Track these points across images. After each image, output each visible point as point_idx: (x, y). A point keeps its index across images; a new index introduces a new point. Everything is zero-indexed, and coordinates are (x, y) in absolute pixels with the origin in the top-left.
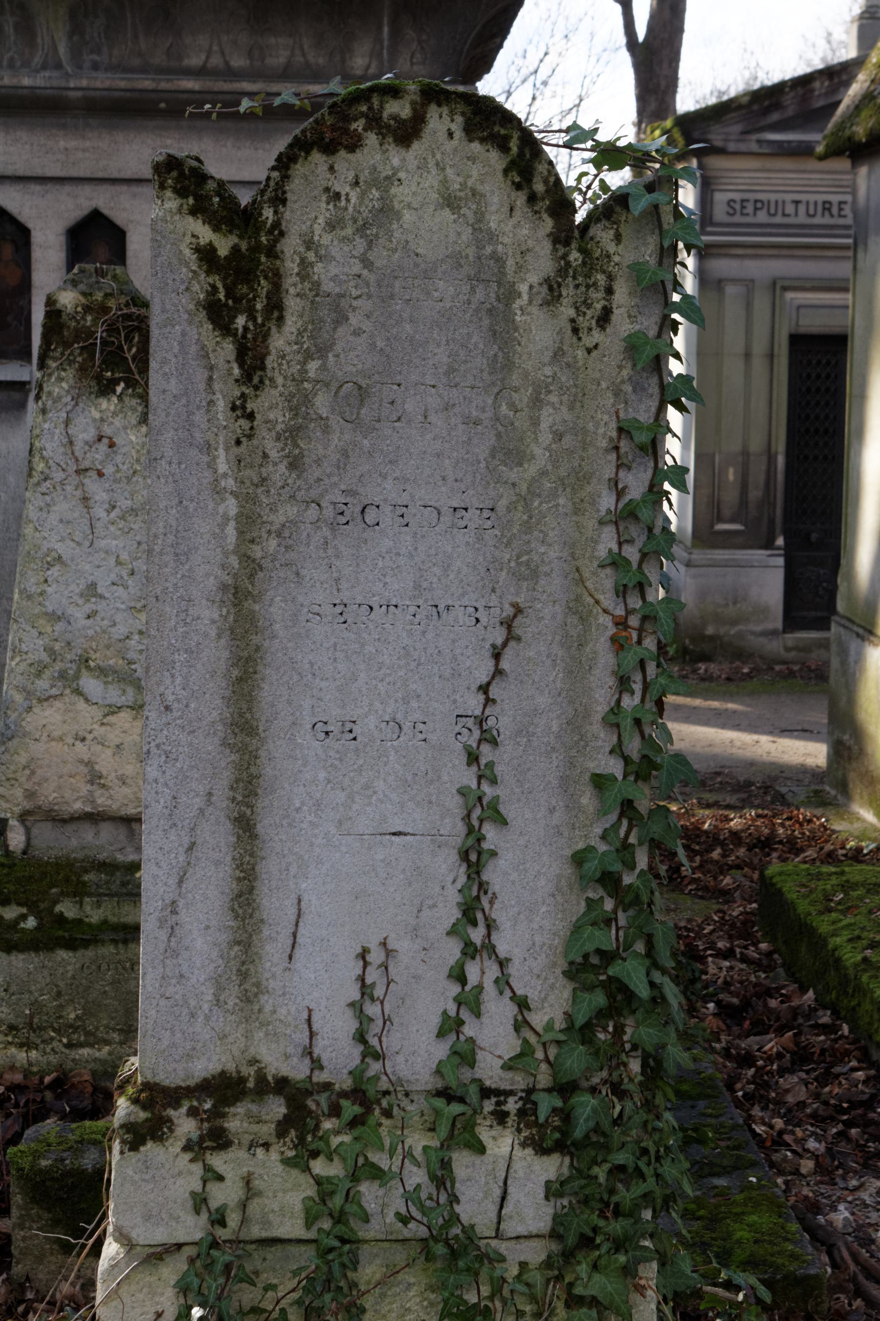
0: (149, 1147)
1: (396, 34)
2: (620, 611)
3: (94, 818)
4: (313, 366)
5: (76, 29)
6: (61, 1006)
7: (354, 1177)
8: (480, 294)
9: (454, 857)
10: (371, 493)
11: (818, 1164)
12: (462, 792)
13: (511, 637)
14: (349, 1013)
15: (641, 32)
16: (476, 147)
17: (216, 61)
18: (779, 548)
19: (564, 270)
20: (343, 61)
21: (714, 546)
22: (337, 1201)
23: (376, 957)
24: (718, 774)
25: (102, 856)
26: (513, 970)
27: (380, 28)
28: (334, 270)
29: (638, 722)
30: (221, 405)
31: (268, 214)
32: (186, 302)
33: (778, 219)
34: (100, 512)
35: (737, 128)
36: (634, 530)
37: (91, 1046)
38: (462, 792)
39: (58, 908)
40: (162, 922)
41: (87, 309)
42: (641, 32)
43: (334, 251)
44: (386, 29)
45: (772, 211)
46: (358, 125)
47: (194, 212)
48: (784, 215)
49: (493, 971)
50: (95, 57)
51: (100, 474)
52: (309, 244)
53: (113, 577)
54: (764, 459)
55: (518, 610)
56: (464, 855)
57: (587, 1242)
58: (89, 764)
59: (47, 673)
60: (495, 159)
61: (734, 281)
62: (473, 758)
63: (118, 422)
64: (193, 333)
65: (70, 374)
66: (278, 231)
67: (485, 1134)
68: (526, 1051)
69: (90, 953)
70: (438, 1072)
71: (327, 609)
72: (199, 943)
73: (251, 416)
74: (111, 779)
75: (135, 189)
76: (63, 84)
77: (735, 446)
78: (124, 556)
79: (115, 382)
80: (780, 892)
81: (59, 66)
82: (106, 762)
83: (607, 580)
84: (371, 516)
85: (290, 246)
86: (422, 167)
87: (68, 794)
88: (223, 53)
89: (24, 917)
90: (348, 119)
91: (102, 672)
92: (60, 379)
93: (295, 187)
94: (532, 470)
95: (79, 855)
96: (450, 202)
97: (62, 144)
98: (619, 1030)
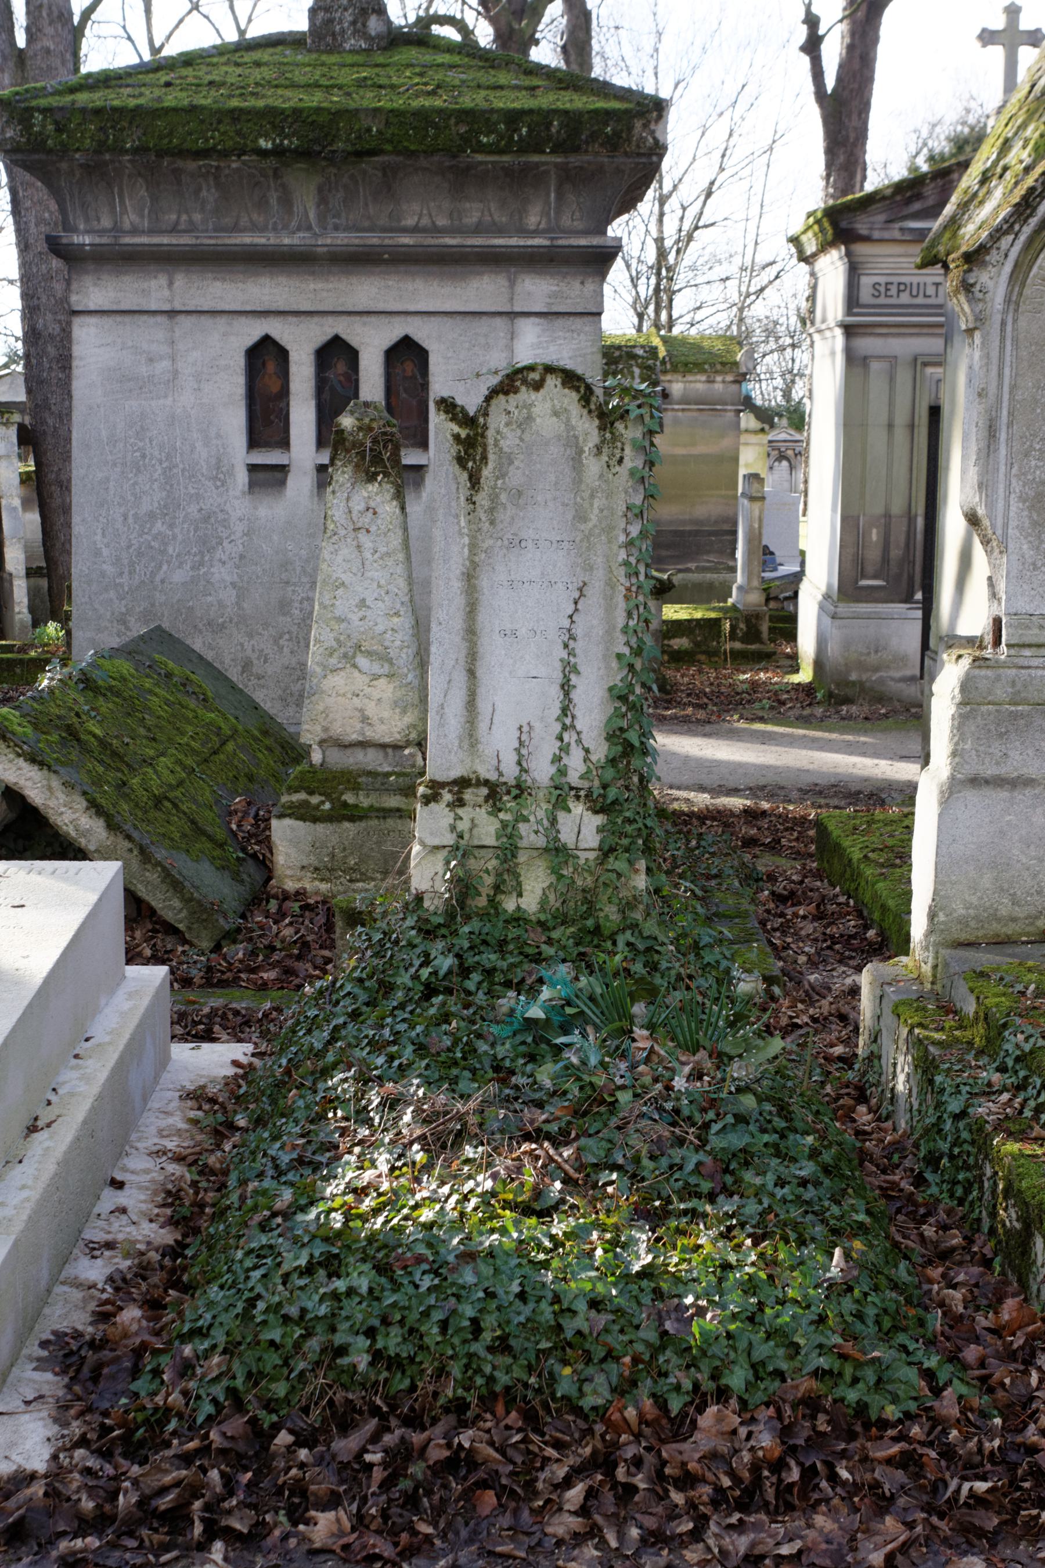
0: (432, 805)
1: (560, 196)
2: (628, 584)
3: (363, 745)
4: (500, 482)
5: (323, 200)
6: (345, 857)
7: (516, 821)
8: (568, 452)
9: (558, 688)
10: (523, 535)
11: (809, 959)
12: (562, 660)
13: (582, 595)
14: (514, 753)
15: (830, 82)
16: (566, 391)
17: (425, 221)
18: (917, 602)
19: (603, 442)
20: (521, 219)
21: (858, 600)
22: (509, 829)
23: (525, 729)
24: (834, 786)
25: (369, 768)
26: (583, 736)
27: (548, 195)
28: (508, 443)
29: (635, 631)
30: (462, 499)
31: (481, 420)
32: (449, 457)
33: (920, 300)
34: (368, 555)
35: (881, 218)
36: (634, 551)
37: (364, 881)
38: (562, 660)
39: (344, 797)
40: (438, 712)
41: (360, 429)
42: (830, 82)
43: (509, 435)
44: (553, 195)
45: (914, 293)
46: (518, 383)
47: (451, 420)
48: (925, 296)
49: (575, 737)
50: (336, 220)
51: (368, 531)
52: (498, 432)
53: (376, 595)
54: (905, 521)
55: (585, 584)
56: (562, 686)
57: (612, 850)
58: (361, 710)
59: (336, 655)
60: (574, 396)
61: (879, 358)
62: (566, 646)
63: (378, 499)
64: (451, 469)
65: (349, 469)
66: (485, 427)
67: (571, 805)
68: (589, 771)
69: (363, 824)
70: (552, 779)
71: (505, 583)
72: (453, 722)
73: (474, 503)
74: (375, 720)
75: (365, 319)
76: (313, 242)
77: (879, 510)
78: (383, 582)
79: (376, 474)
80: (826, 828)
81: (309, 228)
82: (371, 709)
83: (622, 571)
84: (523, 544)
85: (490, 433)
86: (544, 399)
87: (349, 730)
88: (430, 216)
89: (323, 802)
90: (513, 381)
91: (369, 654)
92: (344, 472)
93: (492, 410)
94: (590, 525)
95: (355, 768)
96: (556, 414)
97: (312, 286)
98: (629, 763)
